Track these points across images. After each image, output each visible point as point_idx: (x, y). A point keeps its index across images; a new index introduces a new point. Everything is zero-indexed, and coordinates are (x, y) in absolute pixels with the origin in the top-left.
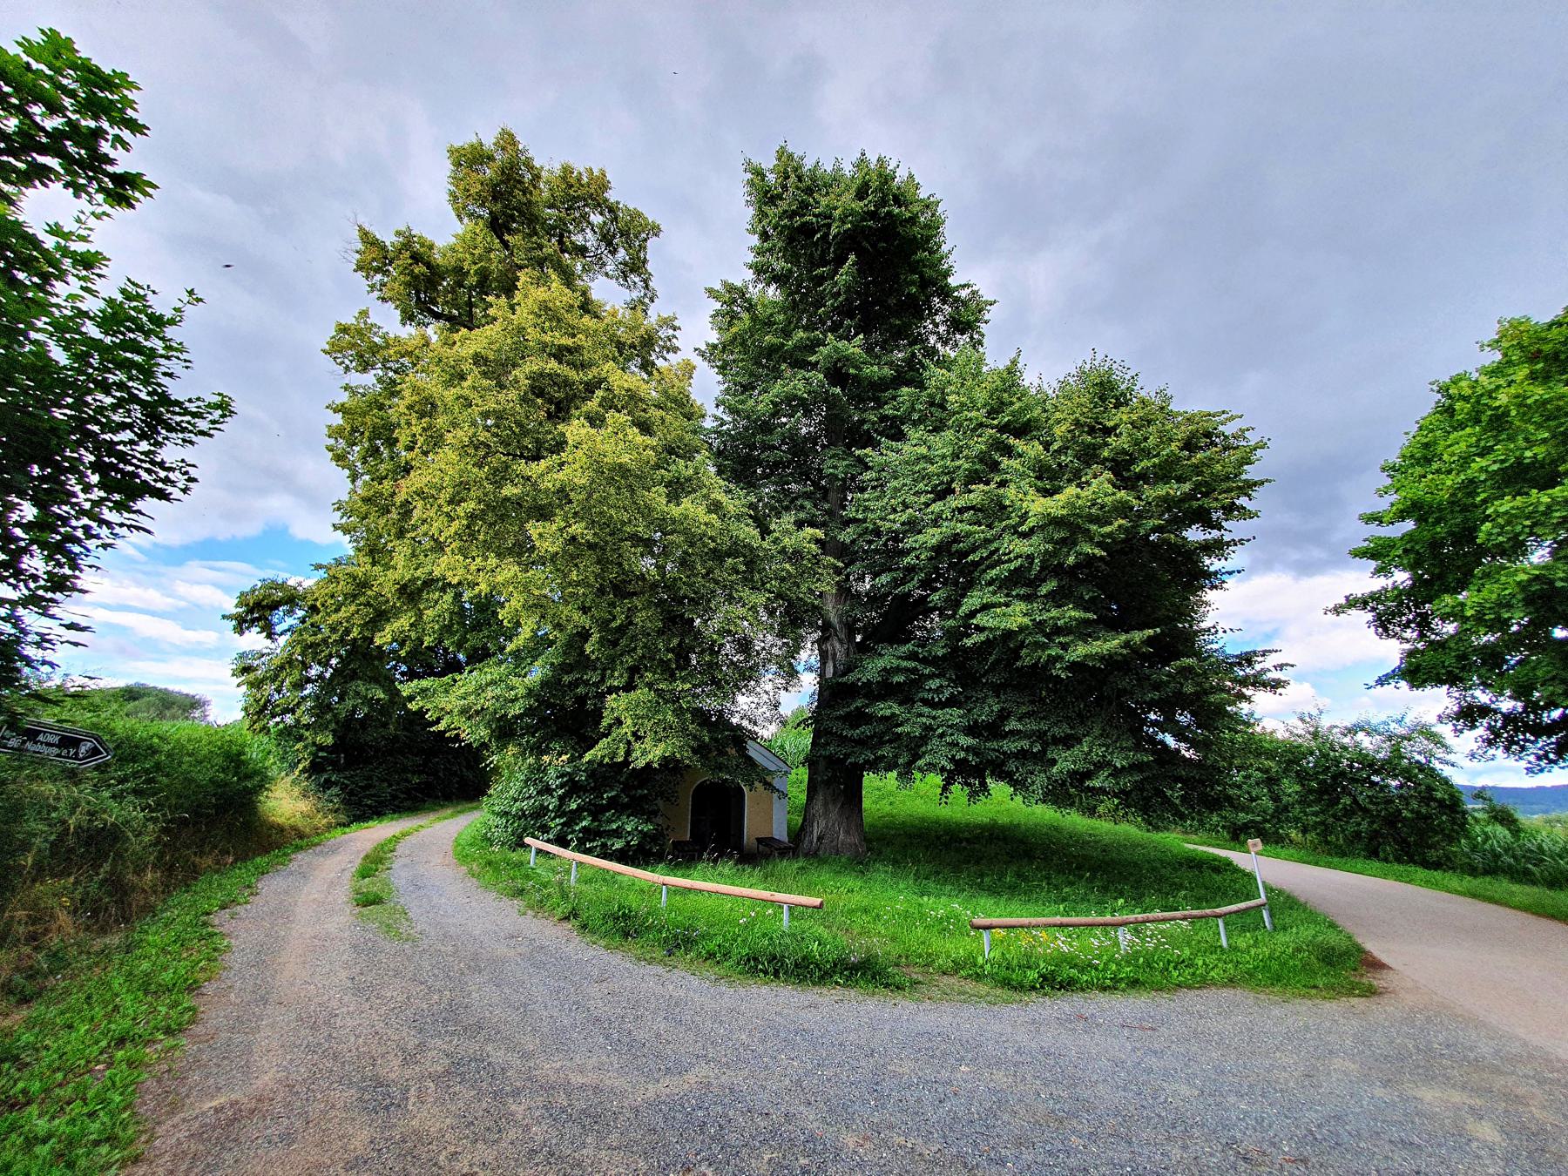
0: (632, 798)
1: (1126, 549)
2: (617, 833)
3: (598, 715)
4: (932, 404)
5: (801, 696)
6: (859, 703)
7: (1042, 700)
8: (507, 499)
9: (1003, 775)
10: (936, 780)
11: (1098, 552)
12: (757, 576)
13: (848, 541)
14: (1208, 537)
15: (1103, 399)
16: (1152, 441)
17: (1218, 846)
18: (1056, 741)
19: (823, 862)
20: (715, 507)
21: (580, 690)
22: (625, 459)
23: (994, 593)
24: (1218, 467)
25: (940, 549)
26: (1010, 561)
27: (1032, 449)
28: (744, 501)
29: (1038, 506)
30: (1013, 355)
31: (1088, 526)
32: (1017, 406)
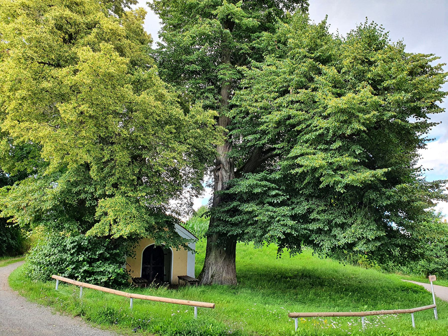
0: (111, 254)
1: (377, 128)
2: (102, 273)
3: (92, 210)
4: (279, 42)
5: (204, 201)
6: (235, 204)
7: (331, 205)
8: (43, 89)
9: (310, 243)
10: (275, 246)
11: (363, 128)
12: (182, 136)
13: (231, 117)
14: (418, 121)
15: (370, 45)
16: (393, 70)
17: (419, 281)
18: (337, 225)
19: (214, 288)
20: (160, 98)
21: (82, 196)
22: (112, 70)
23: (308, 147)
24: (426, 85)
25: (279, 123)
26: (316, 130)
27: (330, 71)
28: (175, 94)
29: (333, 103)
30: (323, 19)
31: (358, 114)
32: (325, 47)
